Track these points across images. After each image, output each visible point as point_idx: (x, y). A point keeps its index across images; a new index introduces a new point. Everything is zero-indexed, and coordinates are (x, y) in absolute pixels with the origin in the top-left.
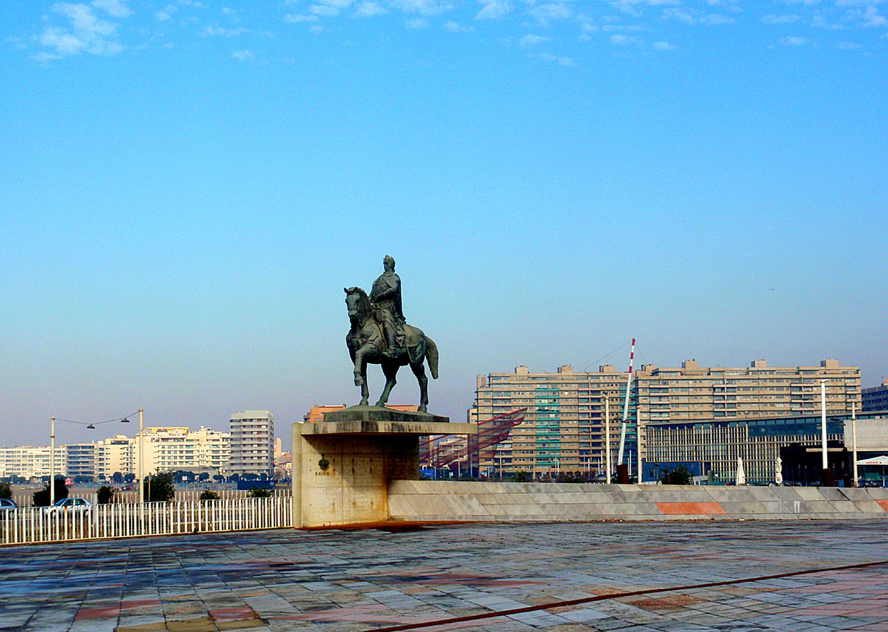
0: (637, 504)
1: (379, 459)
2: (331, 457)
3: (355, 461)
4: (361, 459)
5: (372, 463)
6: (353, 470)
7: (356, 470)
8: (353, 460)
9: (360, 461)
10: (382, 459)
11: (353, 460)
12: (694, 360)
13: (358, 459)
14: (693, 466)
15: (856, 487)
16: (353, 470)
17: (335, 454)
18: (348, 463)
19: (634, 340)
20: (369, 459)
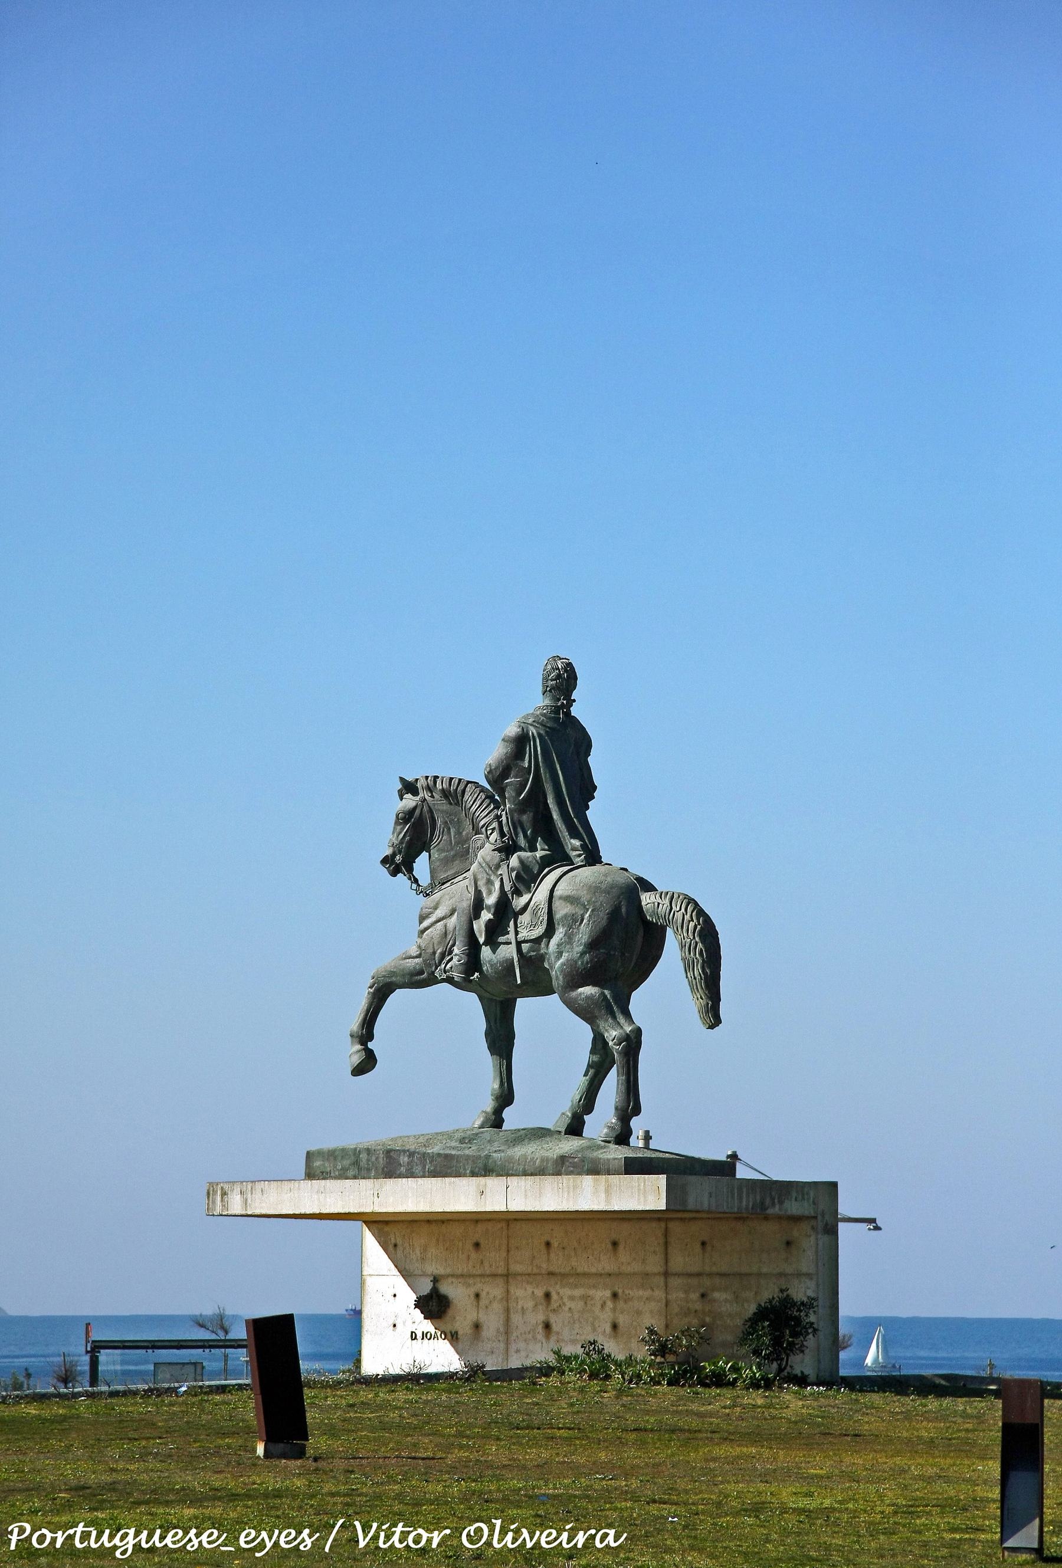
0: (889, 1349)
1: (648, 1293)
2: (468, 1286)
3: (554, 1296)
4: (578, 1292)
5: (621, 1304)
6: (547, 1326)
7: (555, 1327)
8: (548, 1296)
9: (572, 1298)
10: (659, 1294)
11: (548, 1296)
12: (477, 1245)
13: (566, 1292)
14: (779, 1333)
15: (408, 1543)
16: (547, 1326)
17: (482, 1276)
18: (530, 1304)
19: (1052, 1248)
20: (608, 1293)
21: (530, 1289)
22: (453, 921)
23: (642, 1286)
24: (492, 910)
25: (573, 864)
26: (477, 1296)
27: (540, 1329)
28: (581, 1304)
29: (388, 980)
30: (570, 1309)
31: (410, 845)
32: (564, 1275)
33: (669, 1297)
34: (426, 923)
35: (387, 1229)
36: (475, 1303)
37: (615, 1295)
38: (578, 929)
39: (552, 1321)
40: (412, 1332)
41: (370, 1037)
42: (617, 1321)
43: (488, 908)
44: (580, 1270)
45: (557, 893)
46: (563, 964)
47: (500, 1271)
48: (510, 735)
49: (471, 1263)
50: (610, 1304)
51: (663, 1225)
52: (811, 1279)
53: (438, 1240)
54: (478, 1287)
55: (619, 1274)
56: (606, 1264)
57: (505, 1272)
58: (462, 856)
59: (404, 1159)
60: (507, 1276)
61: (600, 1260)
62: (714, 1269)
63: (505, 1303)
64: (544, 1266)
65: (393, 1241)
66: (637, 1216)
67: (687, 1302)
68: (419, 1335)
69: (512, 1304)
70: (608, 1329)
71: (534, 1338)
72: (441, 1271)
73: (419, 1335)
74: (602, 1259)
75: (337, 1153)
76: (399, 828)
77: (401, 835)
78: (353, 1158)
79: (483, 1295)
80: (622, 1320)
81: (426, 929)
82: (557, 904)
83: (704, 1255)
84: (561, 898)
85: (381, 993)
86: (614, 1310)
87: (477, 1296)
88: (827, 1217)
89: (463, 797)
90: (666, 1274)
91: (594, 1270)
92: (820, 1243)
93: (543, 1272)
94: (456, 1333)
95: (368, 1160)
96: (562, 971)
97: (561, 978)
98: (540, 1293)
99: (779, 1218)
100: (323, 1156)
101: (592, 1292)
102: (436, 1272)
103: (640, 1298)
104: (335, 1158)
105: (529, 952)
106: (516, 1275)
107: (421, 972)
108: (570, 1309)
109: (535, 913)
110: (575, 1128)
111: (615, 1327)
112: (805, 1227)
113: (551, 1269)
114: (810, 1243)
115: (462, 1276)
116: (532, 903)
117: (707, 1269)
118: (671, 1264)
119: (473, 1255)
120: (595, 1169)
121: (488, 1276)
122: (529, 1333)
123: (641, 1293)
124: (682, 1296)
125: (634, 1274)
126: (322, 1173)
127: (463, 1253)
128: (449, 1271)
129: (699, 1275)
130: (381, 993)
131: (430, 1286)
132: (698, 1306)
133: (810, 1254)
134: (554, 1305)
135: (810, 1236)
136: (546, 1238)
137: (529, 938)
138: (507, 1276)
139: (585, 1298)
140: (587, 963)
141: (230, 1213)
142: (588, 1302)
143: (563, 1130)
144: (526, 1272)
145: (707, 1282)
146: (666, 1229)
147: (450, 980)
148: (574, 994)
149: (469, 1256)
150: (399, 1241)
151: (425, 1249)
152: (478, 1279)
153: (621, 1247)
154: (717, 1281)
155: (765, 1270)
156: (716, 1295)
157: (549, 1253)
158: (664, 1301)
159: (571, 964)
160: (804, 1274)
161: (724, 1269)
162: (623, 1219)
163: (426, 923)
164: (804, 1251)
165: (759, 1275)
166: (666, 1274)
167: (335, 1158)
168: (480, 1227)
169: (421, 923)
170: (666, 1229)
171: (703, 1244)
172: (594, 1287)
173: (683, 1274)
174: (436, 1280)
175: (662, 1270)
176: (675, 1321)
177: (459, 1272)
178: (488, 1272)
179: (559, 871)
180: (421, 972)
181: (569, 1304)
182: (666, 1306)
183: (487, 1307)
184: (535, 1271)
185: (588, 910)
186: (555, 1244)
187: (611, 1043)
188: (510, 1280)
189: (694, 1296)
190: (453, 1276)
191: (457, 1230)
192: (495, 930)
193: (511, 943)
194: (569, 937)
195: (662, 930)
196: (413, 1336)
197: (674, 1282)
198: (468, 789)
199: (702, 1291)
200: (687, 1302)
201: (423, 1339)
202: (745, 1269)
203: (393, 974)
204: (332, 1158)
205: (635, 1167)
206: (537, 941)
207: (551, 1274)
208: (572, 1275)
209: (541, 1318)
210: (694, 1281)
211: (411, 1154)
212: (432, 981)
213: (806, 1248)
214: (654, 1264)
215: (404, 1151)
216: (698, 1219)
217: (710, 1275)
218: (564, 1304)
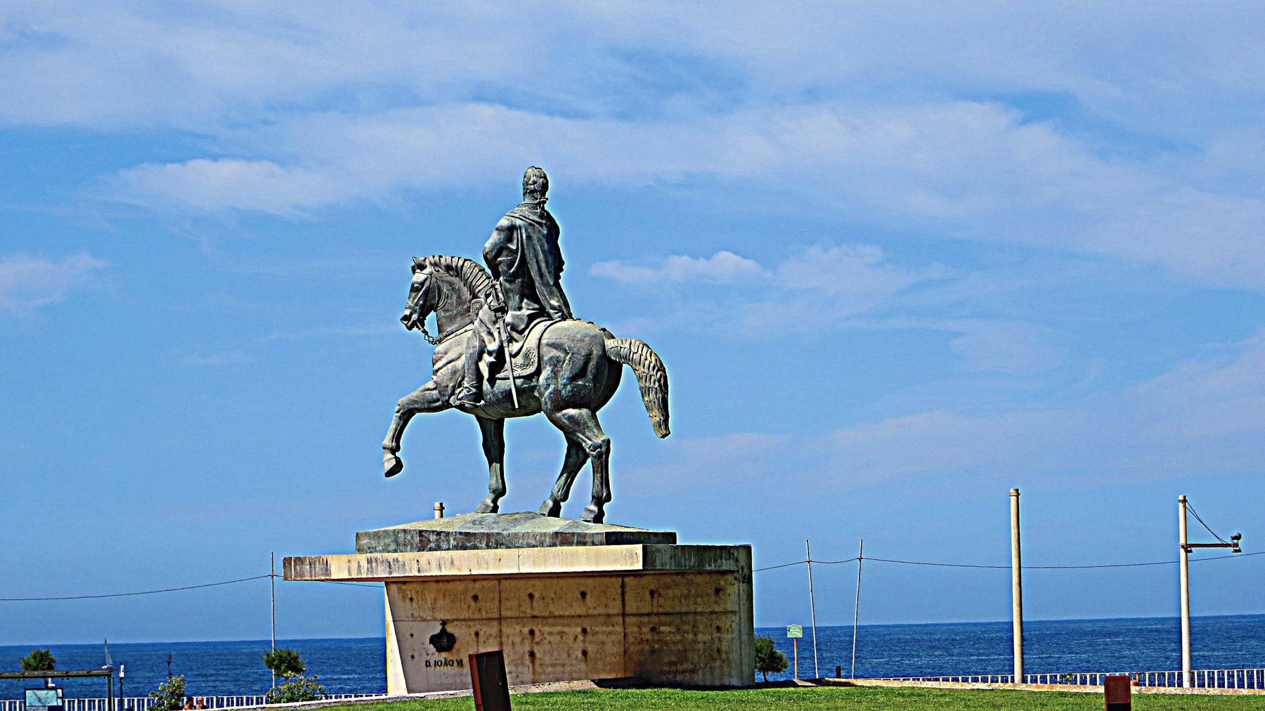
3: (537, 632)
5: (589, 637)
6: (532, 654)
8: (532, 632)
9: (550, 634)
11: (532, 632)
13: (547, 629)
16: (532, 654)
18: (518, 640)
20: (579, 630)
21: (518, 628)
22: (459, 363)
23: (606, 624)
24: (494, 355)
25: (553, 320)
26: (477, 634)
27: (527, 657)
28: (558, 638)
29: (411, 407)
30: (550, 642)
31: (422, 307)
32: (544, 618)
33: (627, 631)
34: (436, 367)
35: (404, 587)
36: (475, 639)
37: (584, 631)
38: (561, 367)
39: (536, 651)
40: (426, 661)
41: (398, 448)
42: (586, 649)
43: (490, 353)
44: (556, 613)
45: (544, 341)
46: (551, 393)
47: (494, 616)
48: (503, 225)
49: (471, 612)
50: (581, 637)
51: (620, 579)
52: (735, 615)
53: (444, 595)
54: (477, 627)
55: (587, 616)
56: (578, 609)
57: (497, 616)
58: (462, 315)
59: (433, 538)
60: (500, 619)
61: (572, 606)
62: (661, 610)
63: (498, 639)
64: (529, 611)
65: (409, 596)
66: (547, 575)
67: (641, 634)
68: (432, 663)
69: (504, 639)
70: (580, 655)
71: (523, 664)
72: (448, 617)
73: (432, 663)
74: (574, 605)
75: (380, 534)
76: (414, 294)
77: (416, 300)
78: (393, 537)
79: (481, 633)
80: (590, 649)
81: (440, 369)
82: (544, 349)
83: (652, 601)
84: (547, 345)
85: (406, 415)
86: (584, 641)
87: (477, 634)
88: (745, 570)
89: (462, 271)
90: (624, 615)
91: (567, 613)
92: (741, 588)
93: (528, 615)
94: (461, 661)
95: (405, 538)
96: (550, 398)
97: (549, 403)
98: (526, 630)
99: (710, 573)
100: (370, 537)
101: (566, 629)
102: (443, 618)
103: (604, 633)
104: (379, 538)
105: (522, 384)
106: (507, 618)
107: (437, 400)
108: (550, 642)
109: (526, 356)
110: (555, 512)
111: (585, 653)
112: (730, 577)
113: (536, 613)
114: (734, 589)
115: (464, 620)
116: (524, 349)
117: (655, 610)
118: (627, 608)
119: (473, 604)
120: (582, 540)
121: (486, 619)
122: (518, 659)
123: (604, 629)
124: (637, 630)
125: (599, 615)
126: (369, 548)
127: (464, 604)
128: (454, 617)
129: (649, 614)
130: (406, 415)
131: (440, 627)
132: (649, 637)
133: (734, 598)
134: (537, 639)
135: (734, 584)
136: (530, 591)
137: (523, 374)
138: (500, 619)
139: (561, 633)
140: (569, 392)
141: (333, 577)
142: (563, 636)
143: (547, 513)
144: (514, 616)
145: (655, 619)
146: (623, 582)
147: (461, 407)
148: (559, 415)
149: (469, 606)
150: (414, 597)
151: (435, 601)
152: (477, 622)
153: (588, 596)
154: (663, 618)
155: (699, 609)
156: (663, 629)
157: (412, 604)
158: (623, 634)
159: (556, 392)
160: (730, 612)
161: (669, 609)
162: (547, 577)
163: (436, 367)
164: (729, 595)
165: (695, 613)
166: (624, 615)
167: (379, 538)
168: (478, 585)
169: (434, 364)
170: (623, 582)
171: (652, 593)
172: (568, 625)
173: (636, 615)
174: (444, 623)
175: (620, 612)
176: (632, 649)
177: (462, 617)
178: (484, 617)
179: (541, 327)
180: (437, 400)
181: (549, 638)
182: (624, 637)
183: (485, 642)
184: (522, 615)
185: (568, 353)
186: (537, 595)
187: (588, 450)
188: (503, 622)
189: (646, 630)
190: (457, 620)
191: (459, 587)
192: (496, 368)
193: (509, 379)
194: (555, 374)
195: (618, 367)
196: (428, 664)
197: (629, 620)
198: (466, 264)
199: (651, 626)
200: (641, 634)
201: (435, 665)
202: (684, 609)
203: (415, 402)
204: (376, 538)
205: (613, 539)
206: (528, 378)
207: (534, 617)
208: (550, 617)
209: (527, 648)
210: (645, 619)
211: (439, 534)
212: (447, 405)
213: (731, 593)
214: (615, 608)
215: (433, 532)
216: (455, 580)
217: (658, 614)
218: (545, 638)
